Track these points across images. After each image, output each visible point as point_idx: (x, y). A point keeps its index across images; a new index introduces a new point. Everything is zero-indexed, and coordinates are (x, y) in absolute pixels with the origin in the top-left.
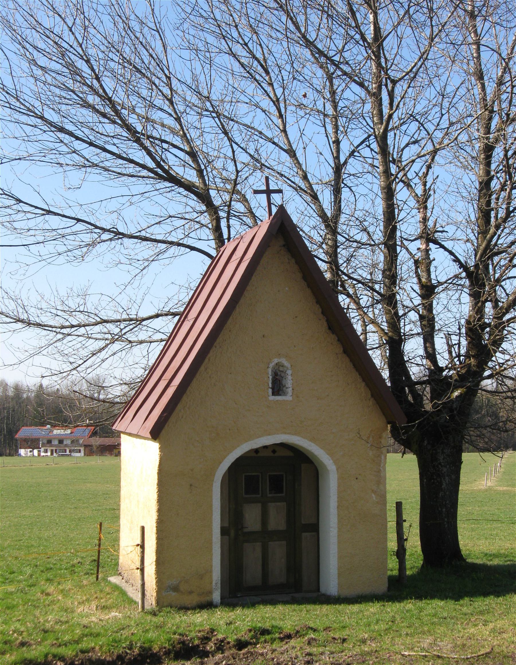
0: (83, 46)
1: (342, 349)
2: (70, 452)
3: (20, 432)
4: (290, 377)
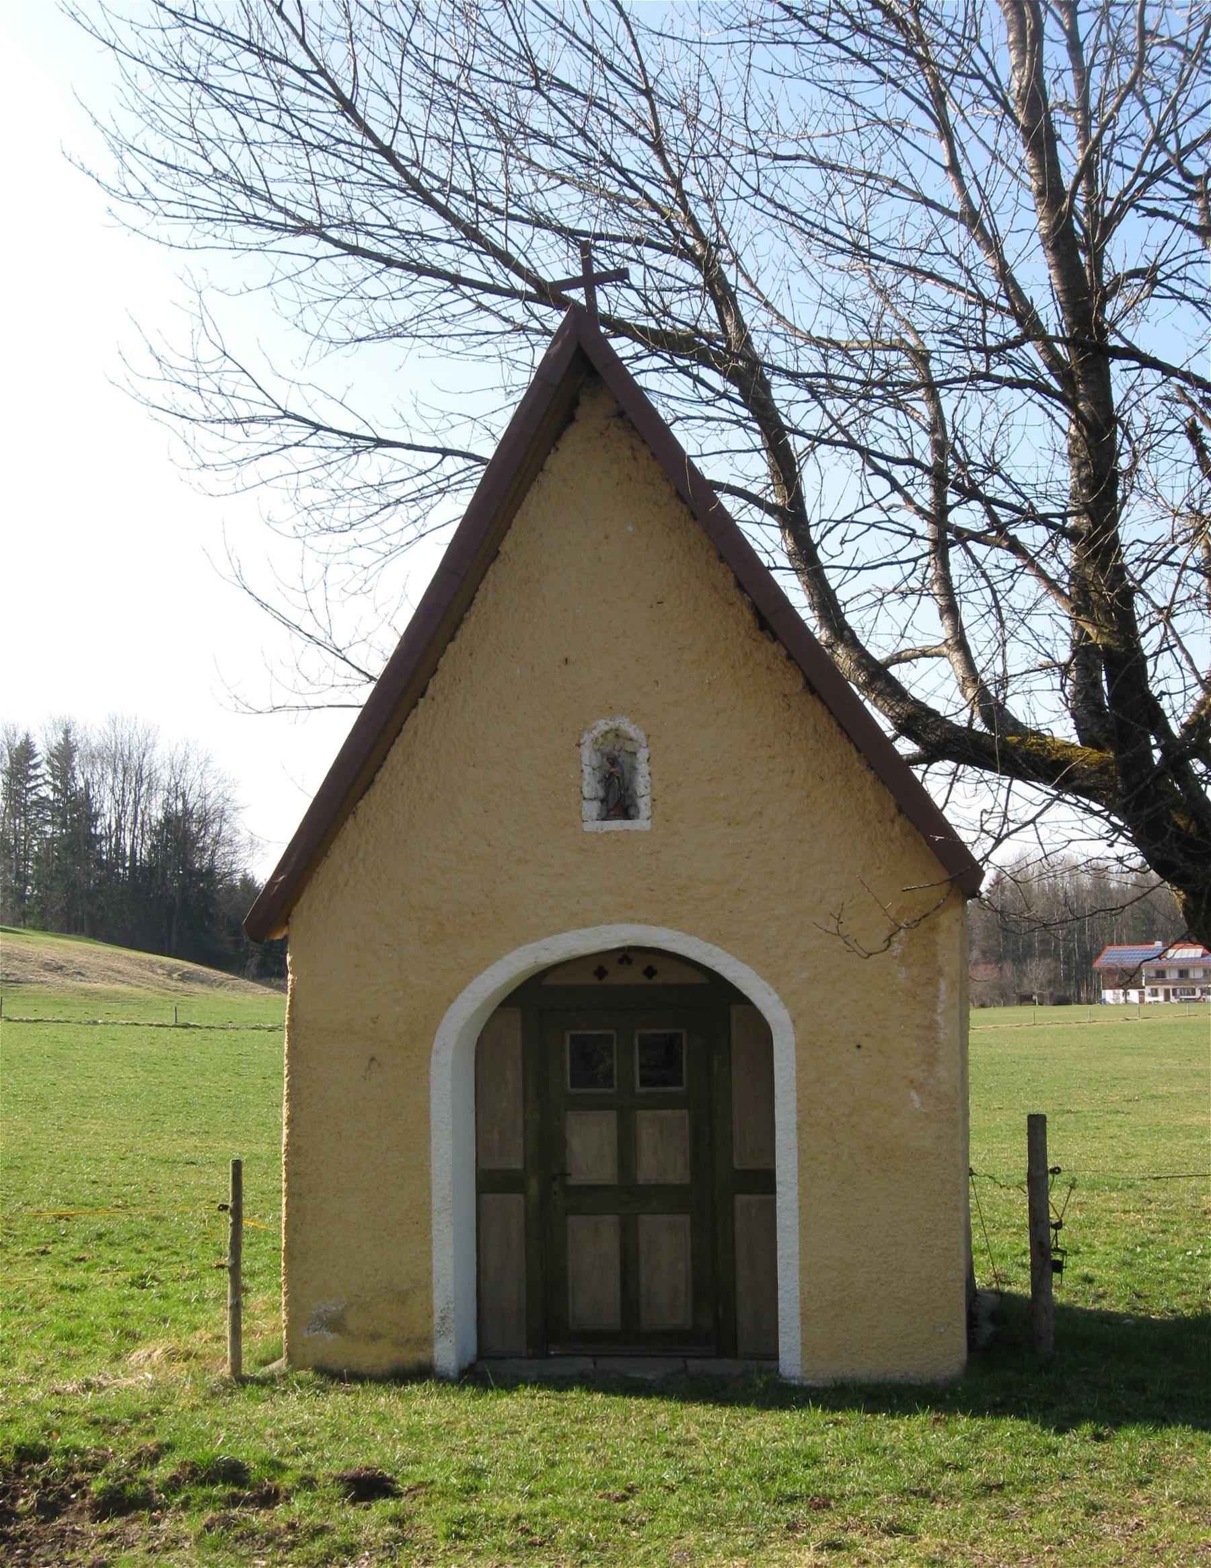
0: (311, 40)
1: (801, 681)
2: (1203, 991)
3: (1102, 956)
4: (643, 768)
